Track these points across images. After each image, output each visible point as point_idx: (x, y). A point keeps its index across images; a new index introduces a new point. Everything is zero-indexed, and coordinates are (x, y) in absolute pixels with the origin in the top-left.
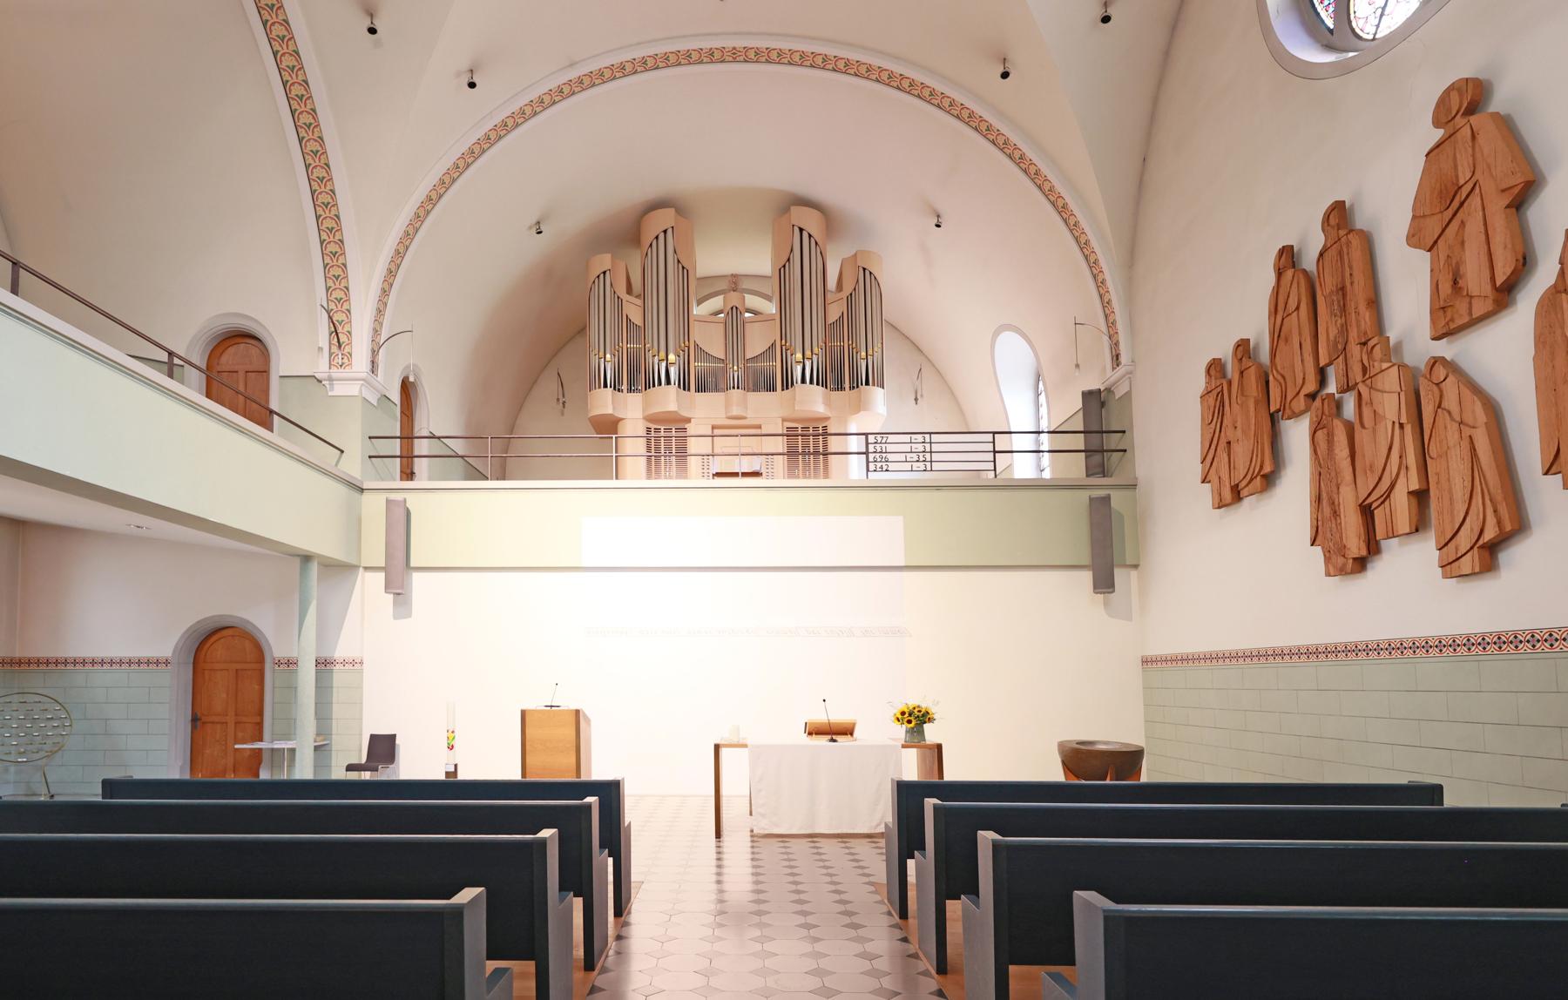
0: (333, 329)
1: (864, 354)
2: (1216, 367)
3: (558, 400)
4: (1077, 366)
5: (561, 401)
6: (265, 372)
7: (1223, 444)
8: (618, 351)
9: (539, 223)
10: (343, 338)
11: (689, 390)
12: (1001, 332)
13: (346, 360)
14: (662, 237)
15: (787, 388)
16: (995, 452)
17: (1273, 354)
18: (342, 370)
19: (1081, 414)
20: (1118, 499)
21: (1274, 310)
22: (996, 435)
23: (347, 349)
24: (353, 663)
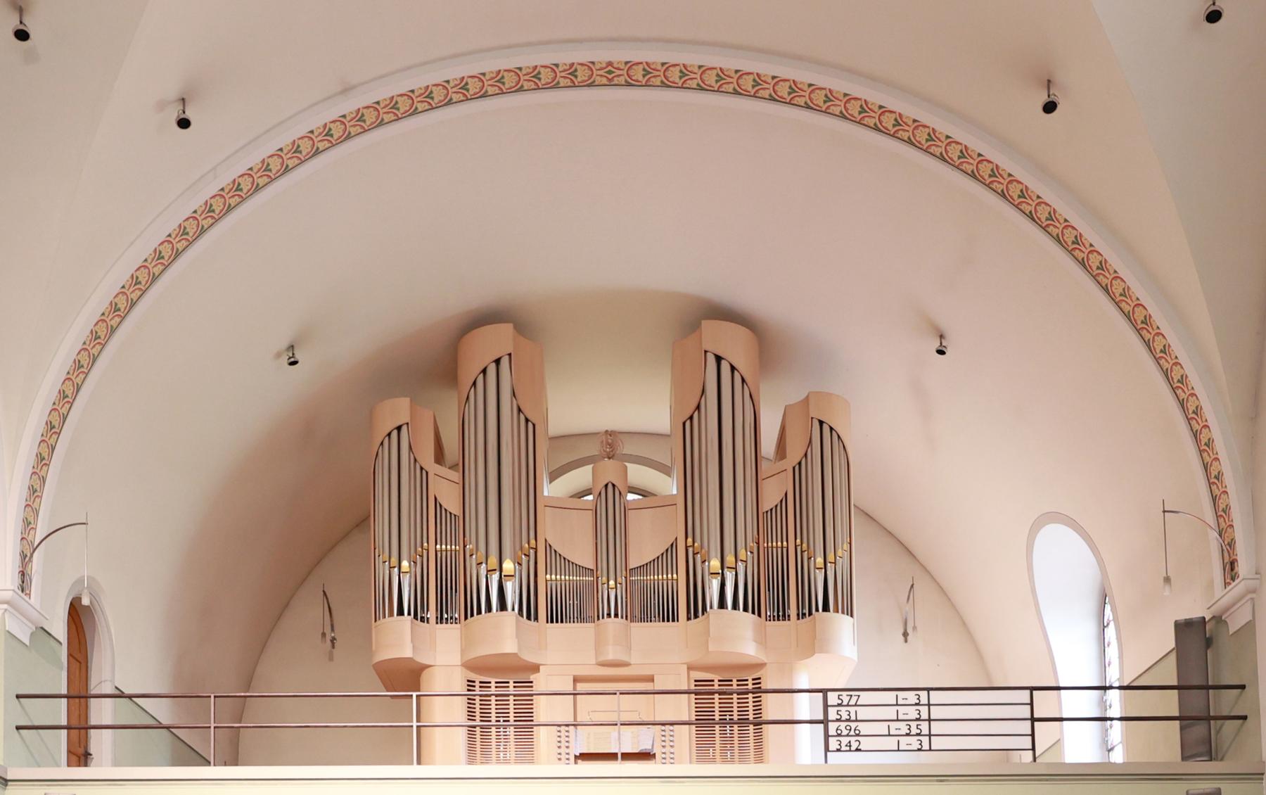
1: (820, 560)
3: (324, 635)
4: (1167, 580)
5: (328, 638)
9: (292, 347)
11: (536, 619)
15: (696, 616)
16: (1033, 720)
19: (1173, 656)
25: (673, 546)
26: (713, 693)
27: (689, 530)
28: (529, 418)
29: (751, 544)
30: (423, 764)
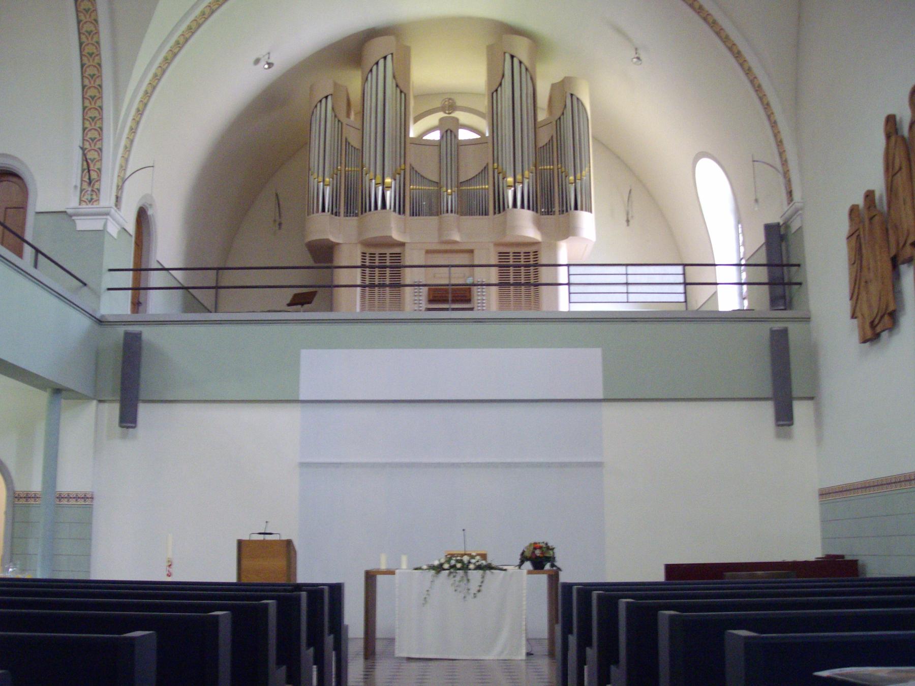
0: (85, 167)
1: (572, 178)
2: (853, 210)
3: (275, 221)
4: (756, 201)
5: (277, 223)
6: (22, 208)
7: (863, 284)
8: (337, 174)
9: (269, 53)
10: (94, 175)
11: (404, 213)
12: (700, 158)
13: (94, 197)
14: (381, 62)
15: (499, 212)
16: (686, 284)
17: (889, 207)
18: (90, 206)
19: (764, 248)
20: (795, 331)
21: (887, 169)
22: (687, 268)
23: (96, 186)
24: (85, 498)
25: (486, 168)
26: (508, 266)
27: (495, 159)
28: (403, 90)
29: (533, 168)
30: (822, 504)
